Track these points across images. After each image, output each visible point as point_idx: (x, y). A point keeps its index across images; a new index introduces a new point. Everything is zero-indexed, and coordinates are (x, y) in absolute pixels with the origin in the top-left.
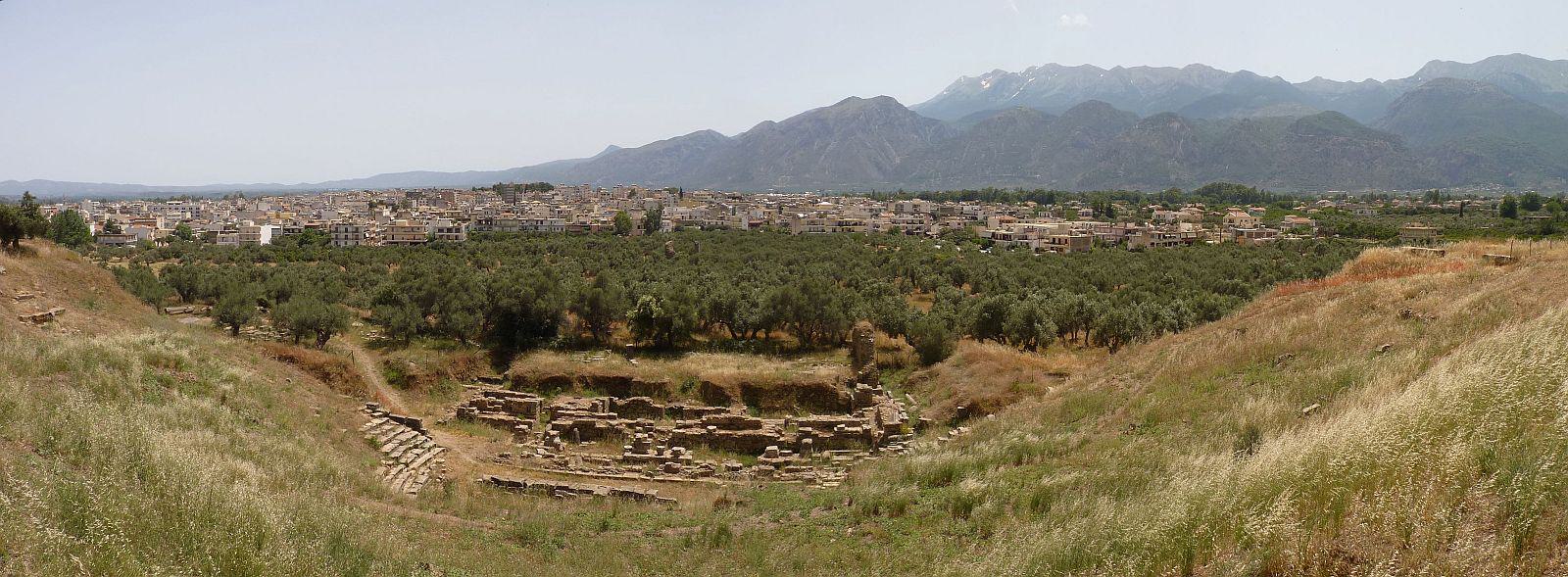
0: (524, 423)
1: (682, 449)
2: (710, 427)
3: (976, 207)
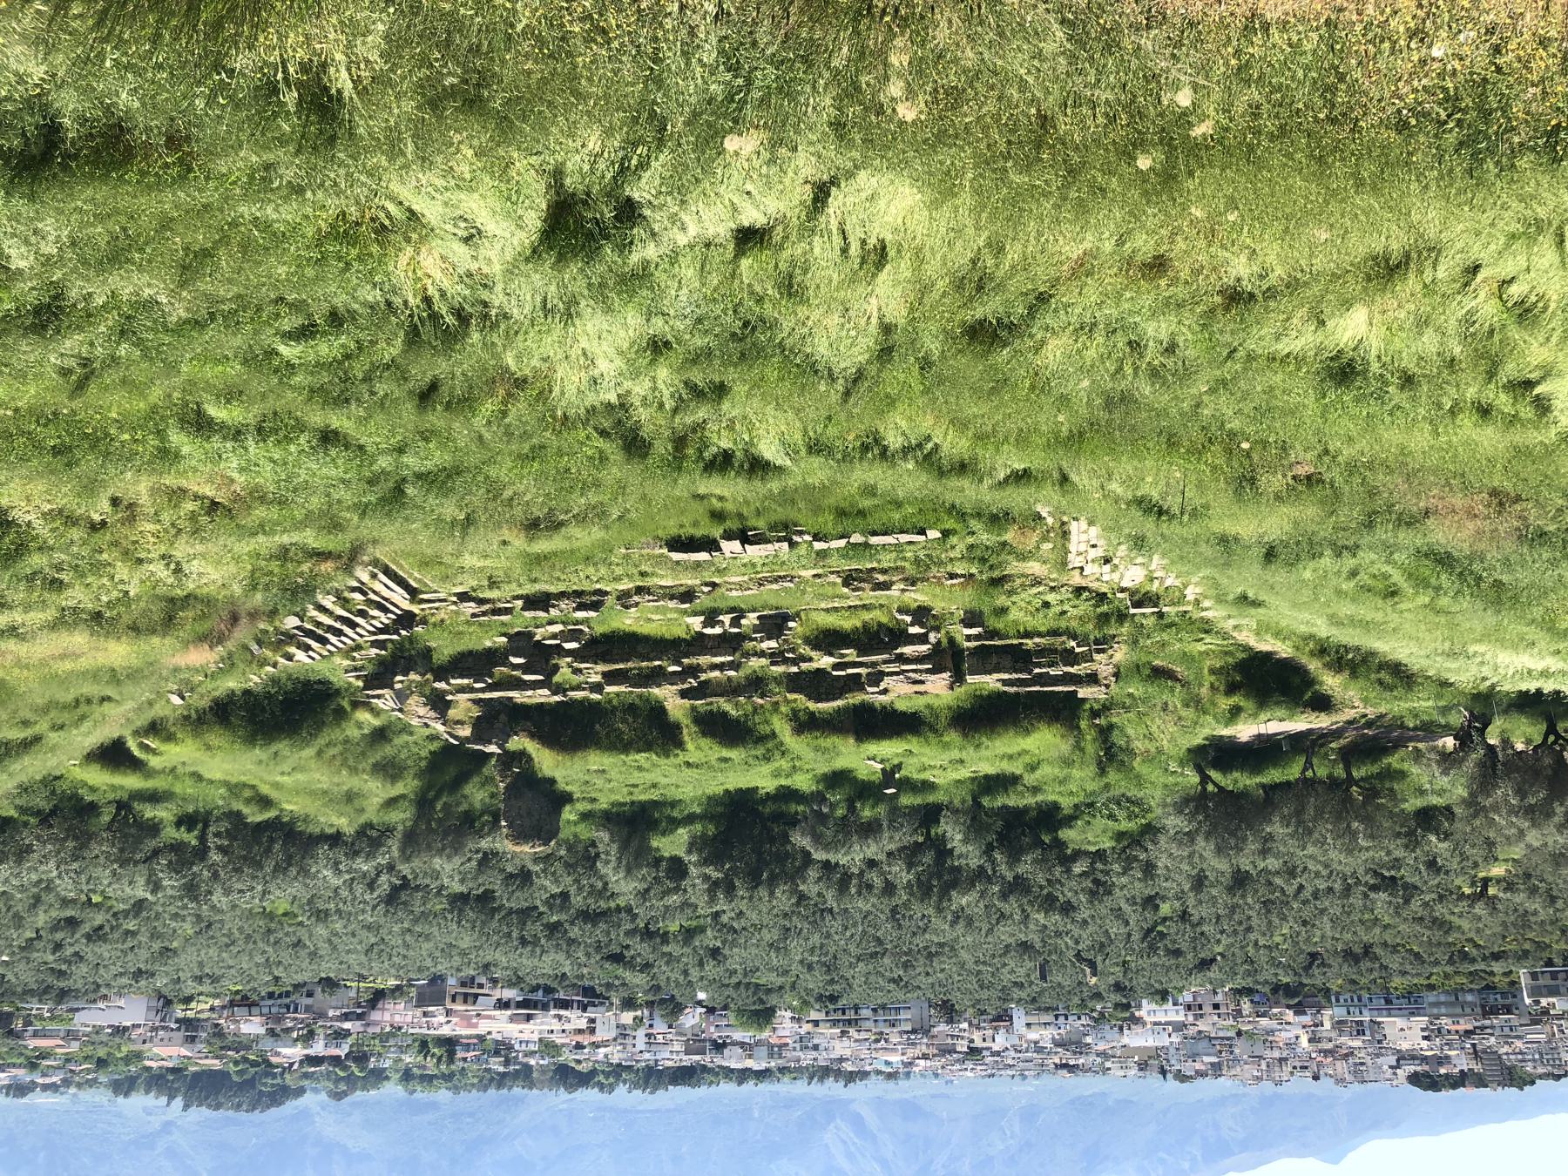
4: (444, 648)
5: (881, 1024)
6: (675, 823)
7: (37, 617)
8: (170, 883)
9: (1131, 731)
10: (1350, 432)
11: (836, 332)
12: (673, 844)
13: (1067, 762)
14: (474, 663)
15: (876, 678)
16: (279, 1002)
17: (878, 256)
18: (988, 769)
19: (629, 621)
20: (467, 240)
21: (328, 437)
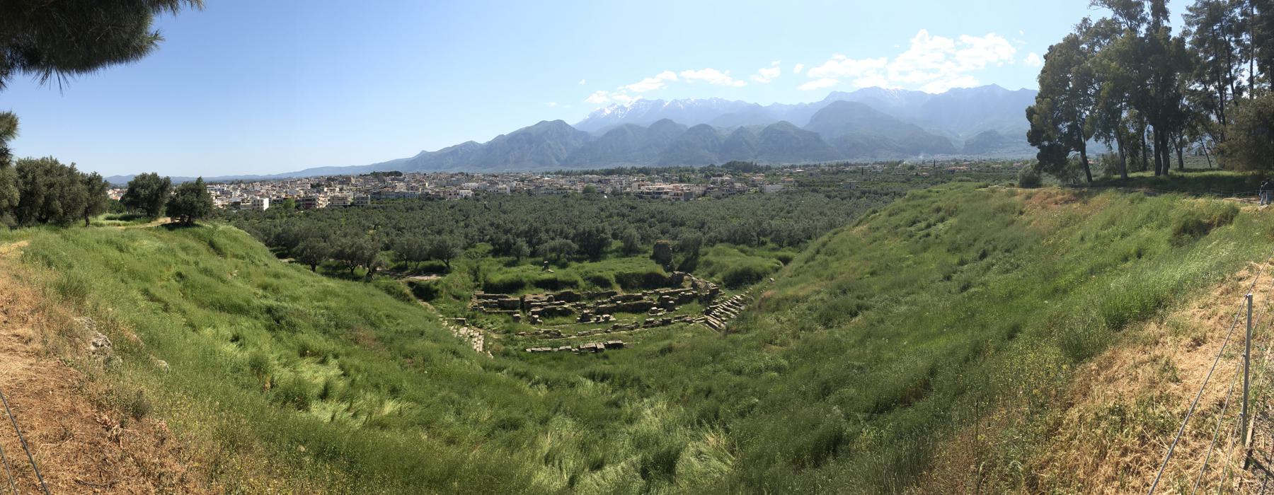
4: (695, 304)
6: (616, 251)
7: (813, 298)
8: (765, 225)
9: (468, 279)
10: (393, 370)
11: (565, 429)
12: (616, 244)
13: (489, 270)
14: (684, 300)
15: (550, 300)
16: (732, 193)
17: (548, 459)
18: (514, 269)
19: (635, 318)
20: (701, 453)
21: (739, 372)
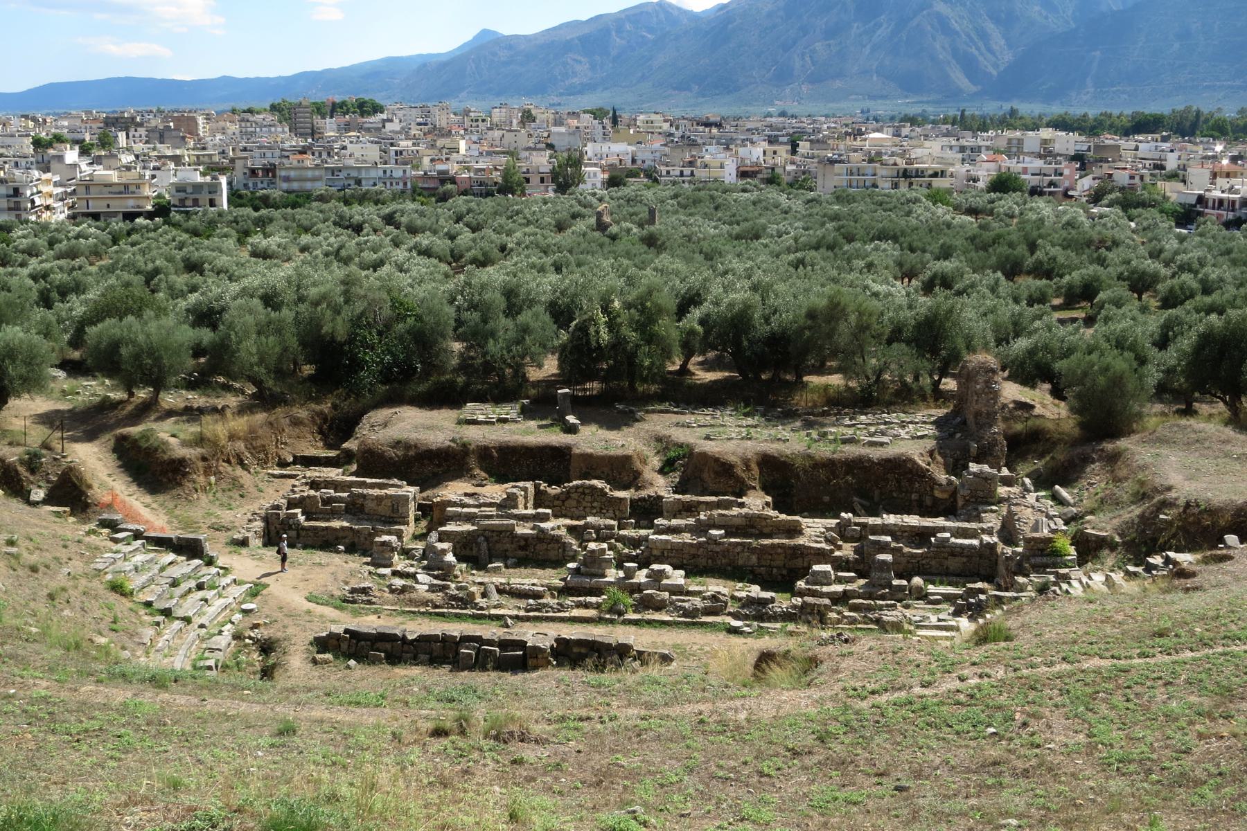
0: (389, 533)
1: (668, 568)
2: (713, 532)
3: (1165, 146)
5: (870, 171)
